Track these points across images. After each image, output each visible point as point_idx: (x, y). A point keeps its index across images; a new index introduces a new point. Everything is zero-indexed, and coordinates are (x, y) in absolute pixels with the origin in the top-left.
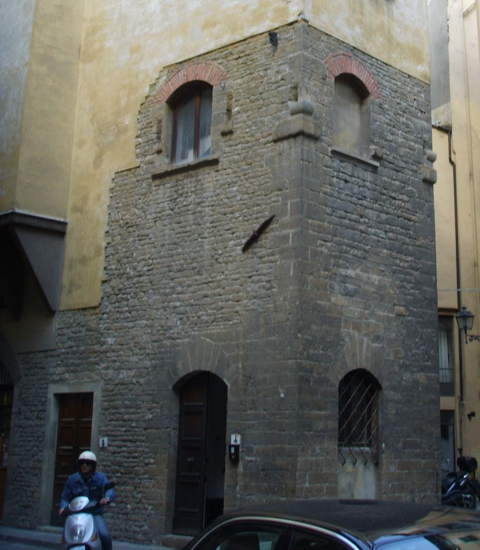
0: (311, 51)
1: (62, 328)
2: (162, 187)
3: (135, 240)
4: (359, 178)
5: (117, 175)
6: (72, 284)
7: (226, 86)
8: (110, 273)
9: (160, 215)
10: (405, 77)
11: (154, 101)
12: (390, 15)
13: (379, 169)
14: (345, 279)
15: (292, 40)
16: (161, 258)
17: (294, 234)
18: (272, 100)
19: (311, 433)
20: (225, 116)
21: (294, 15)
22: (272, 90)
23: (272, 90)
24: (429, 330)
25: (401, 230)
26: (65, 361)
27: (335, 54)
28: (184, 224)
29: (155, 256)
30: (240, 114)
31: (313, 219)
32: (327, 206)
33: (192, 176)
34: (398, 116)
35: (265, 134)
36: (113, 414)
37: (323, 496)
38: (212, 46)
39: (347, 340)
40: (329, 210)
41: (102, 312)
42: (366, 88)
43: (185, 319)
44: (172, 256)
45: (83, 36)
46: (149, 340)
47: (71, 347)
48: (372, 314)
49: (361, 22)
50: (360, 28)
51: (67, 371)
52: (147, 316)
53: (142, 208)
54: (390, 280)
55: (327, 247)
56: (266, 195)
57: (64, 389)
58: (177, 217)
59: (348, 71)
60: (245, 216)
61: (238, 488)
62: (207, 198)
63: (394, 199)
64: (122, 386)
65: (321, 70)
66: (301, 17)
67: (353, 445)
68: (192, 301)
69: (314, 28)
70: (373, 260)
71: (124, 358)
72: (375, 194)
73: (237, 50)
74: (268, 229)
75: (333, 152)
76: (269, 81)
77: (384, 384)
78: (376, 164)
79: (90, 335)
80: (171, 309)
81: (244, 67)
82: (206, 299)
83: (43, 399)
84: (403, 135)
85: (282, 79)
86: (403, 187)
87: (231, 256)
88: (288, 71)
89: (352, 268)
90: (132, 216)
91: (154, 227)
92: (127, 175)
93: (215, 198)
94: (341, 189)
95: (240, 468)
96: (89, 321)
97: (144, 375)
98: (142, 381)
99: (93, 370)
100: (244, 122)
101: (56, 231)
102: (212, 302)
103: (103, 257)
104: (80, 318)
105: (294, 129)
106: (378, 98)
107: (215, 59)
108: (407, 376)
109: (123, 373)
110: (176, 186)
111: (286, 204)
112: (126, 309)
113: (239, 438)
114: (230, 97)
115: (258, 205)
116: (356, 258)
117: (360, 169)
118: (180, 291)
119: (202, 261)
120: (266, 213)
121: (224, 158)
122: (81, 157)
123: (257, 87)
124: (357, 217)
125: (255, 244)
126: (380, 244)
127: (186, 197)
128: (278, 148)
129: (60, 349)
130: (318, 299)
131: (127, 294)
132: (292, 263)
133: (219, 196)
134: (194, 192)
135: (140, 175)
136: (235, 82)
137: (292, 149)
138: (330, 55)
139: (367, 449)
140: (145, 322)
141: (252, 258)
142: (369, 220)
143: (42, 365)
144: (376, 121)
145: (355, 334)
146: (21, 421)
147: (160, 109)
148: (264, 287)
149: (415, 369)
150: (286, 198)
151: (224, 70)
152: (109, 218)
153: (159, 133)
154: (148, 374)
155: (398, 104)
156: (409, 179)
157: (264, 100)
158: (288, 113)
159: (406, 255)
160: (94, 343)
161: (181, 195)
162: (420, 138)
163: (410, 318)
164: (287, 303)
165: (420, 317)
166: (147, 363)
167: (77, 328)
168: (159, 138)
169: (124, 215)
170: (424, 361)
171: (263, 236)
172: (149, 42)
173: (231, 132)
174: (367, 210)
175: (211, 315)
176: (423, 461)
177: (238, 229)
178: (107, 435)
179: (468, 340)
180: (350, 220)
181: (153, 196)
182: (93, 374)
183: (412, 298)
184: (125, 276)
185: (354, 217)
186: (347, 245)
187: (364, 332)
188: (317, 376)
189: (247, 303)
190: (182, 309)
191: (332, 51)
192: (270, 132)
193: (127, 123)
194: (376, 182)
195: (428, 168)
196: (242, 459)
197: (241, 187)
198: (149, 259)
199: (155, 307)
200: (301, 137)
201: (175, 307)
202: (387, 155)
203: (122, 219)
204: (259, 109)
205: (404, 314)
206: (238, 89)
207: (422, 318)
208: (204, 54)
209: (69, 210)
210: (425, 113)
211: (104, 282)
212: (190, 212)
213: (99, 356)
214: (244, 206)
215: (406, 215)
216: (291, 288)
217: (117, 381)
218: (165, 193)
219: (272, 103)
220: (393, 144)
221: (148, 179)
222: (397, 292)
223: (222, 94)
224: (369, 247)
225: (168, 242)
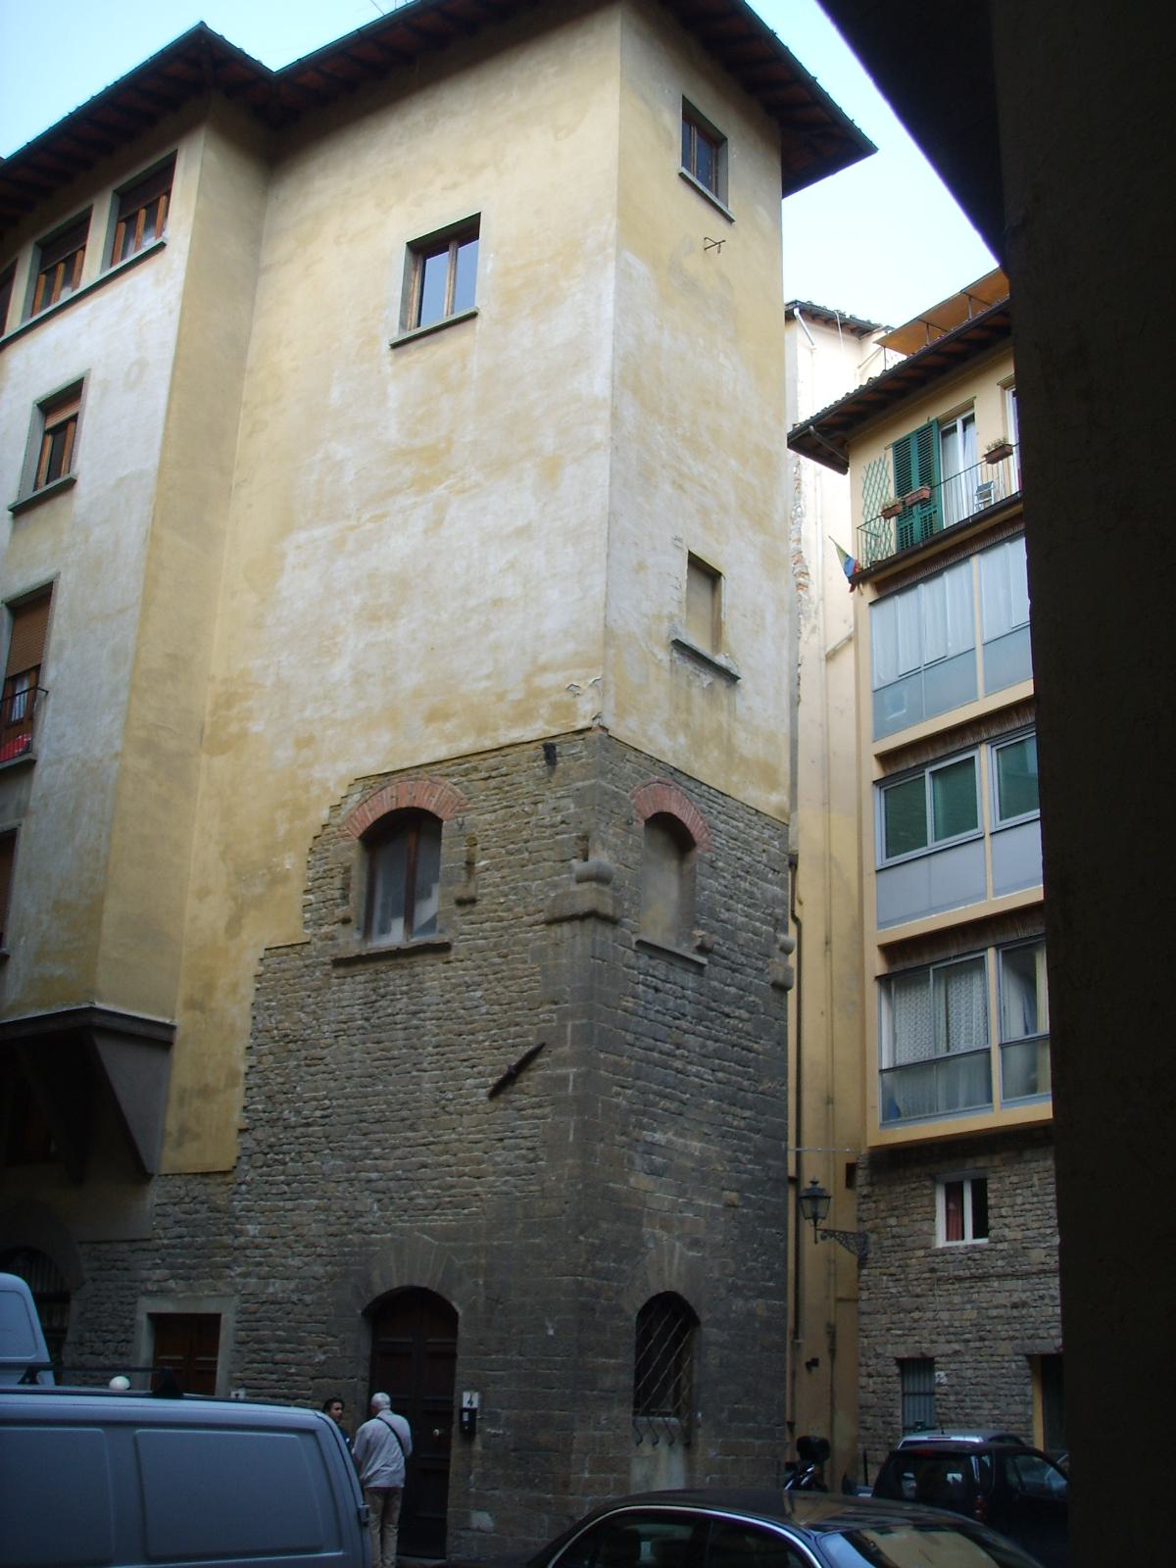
0: (612, 779)
1: (165, 1204)
2: (349, 979)
3: (299, 1066)
4: (675, 984)
5: (268, 952)
6: (184, 1131)
7: (466, 822)
9: (345, 1026)
10: (751, 815)
11: (338, 833)
12: (732, 711)
13: (707, 968)
14: (651, 1147)
15: (580, 758)
16: (346, 1099)
17: (577, 1076)
18: (545, 854)
19: (595, 1393)
20: (463, 872)
21: (585, 717)
22: (544, 838)
23: (544, 838)
24: (774, 1231)
25: (738, 1067)
26: (168, 1260)
27: (648, 781)
28: (387, 1044)
29: (336, 1093)
30: (489, 873)
31: (607, 1052)
32: (627, 1031)
33: (403, 967)
34: (738, 879)
35: (531, 909)
36: (254, 1351)
37: (609, 1493)
38: (442, 752)
39: (651, 1245)
40: (630, 1037)
41: (239, 1181)
42: (691, 835)
43: (386, 1201)
45: (209, 706)
46: (323, 1232)
48: (690, 1204)
49: (686, 726)
50: (686, 736)
52: (319, 1193)
53: (314, 1012)
54: (718, 1149)
55: (626, 1097)
56: (530, 1009)
57: (167, 1307)
58: (374, 1032)
59: (665, 810)
60: (494, 1041)
61: (472, 1477)
62: (429, 1006)
63: (728, 1016)
64: (272, 1306)
65: (625, 810)
66: (597, 721)
67: (653, 1414)
68: (400, 1172)
69: (617, 739)
70: (693, 1117)
72: (699, 1009)
73: (485, 764)
74: (533, 1065)
75: (640, 943)
76: (540, 823)
77: (704, 1316)
78: (703, 960)
79: (216, 1219)
80: (363, 1183)
81: (497, 794)
82: (423, 1170)
83: (127, 1322)
84: (744, 911)
85: (563, 822)
86: (742, 997)
87: (468, 1103)
88: (572, 811)
89: (662, 1131)
90: (295, 1023)
91: (334, 1047)
92: (287, 955)
94: (648, 1002)
96: (214, 1195)
97: (312, 1289)
98: (308, 1298)
99: (220, 1277)
101: (157, 1039)
102: (434, 1176)
103: (240, 1090)
104: (197, 1188)
105: (583, 905)
106: (709, 850)
107: (447, 775)
108: (738, 1304)
109: (274, 1284)
110: (375, 980)
111: (565, 1026)
112: (282, 1178)
113: (476, 1397)
115: (517, 1025)
116: (667, 1113)
117: (678, 970)
118: (377, 1156)
119: (417, 1108)
120: (531, 1039)
121: (461, 942)
122: (204, 916)
123: (518, 831)
124: (672, 1047)
125: (510, 1088)
126: (703, 1090)
127: (392, 1000)
128: (553, 935)
129: (160, 1239)
130: (610, 1181)
131: (284, 1153)
132: (572, 1122)
133: (449, 1005)
134: (406, 993)
135: (311, 957)
136: (482, 817)
137: (577, 939)
138: (638, 783)
139: (674, 1420)
140: (315, 1202)
141: (506, 1109)
142: (689, 1051)
143: (126, 1264)
144: (704, 889)
145: (663, 1236)
146: (85, 1357)
147: (349, 849)
148: (524, 1157)
149: (751, 1294)
150: (565, 1015)
151: (463, 795)
152: (254, 1024)
153: (346, 887)
154: (320, 1288)
155: (739, 859)
156: (751, 982)
157: (530, 853)
158: (572, 878)
159: (742, 1108)
160: (223, 1231)
162: (770, 915)
163: (745, 1211)
164: (562, 1186)
165: (760, 1208)
167: (192, 1205)
168: (345, 897)
169: (281, 1022)
170: (763, 1280)
171: (524, 1075)
172: (330, 732)
173: (473, 901)
174: (687, 1035)
175: (432, 1197)
177: (482, 1061)
178: (246, 1387)
179: (818, 1236)
181: (334, 993)
182: (220, 1284)
183: (750, 1177)
184: (280, 1123)
185: (667, 1047)
186: (656, 1093)
187: (676, 1233)
188: (606, 1302)
189: (495, 1181)
190: (381, 1185)
191: (642, 777)
192: (540, 907)
193: (288, 867)
194: (701, 990)
195: (780, 965)
196: (480, 1431)
197: (489, 992)
198: (325, 1098)
199: (333, 1178)
200: (593, 920)
201: (369, 1181)
202: (719, 944)
203: (277, 1028)
204: (523, 866)
205: (736, 1203)
206: (487, 830)
207: (764, 1210)
209: (179, 1006)
210: (779, 872)
211: (242, 1131)
212: (399, 1026)
213: (231, 1254)
214: (492, 1024)
215: (745, 1043)
216: (570, 1161)
217: (264, 1298)
218: (354, 991)
219: (544, 860)
220: (729, 927)
221: (325, 964)
222: (728, 1169)
223: (459, 836)
224: (688, 1096)
225: (359, 1072)
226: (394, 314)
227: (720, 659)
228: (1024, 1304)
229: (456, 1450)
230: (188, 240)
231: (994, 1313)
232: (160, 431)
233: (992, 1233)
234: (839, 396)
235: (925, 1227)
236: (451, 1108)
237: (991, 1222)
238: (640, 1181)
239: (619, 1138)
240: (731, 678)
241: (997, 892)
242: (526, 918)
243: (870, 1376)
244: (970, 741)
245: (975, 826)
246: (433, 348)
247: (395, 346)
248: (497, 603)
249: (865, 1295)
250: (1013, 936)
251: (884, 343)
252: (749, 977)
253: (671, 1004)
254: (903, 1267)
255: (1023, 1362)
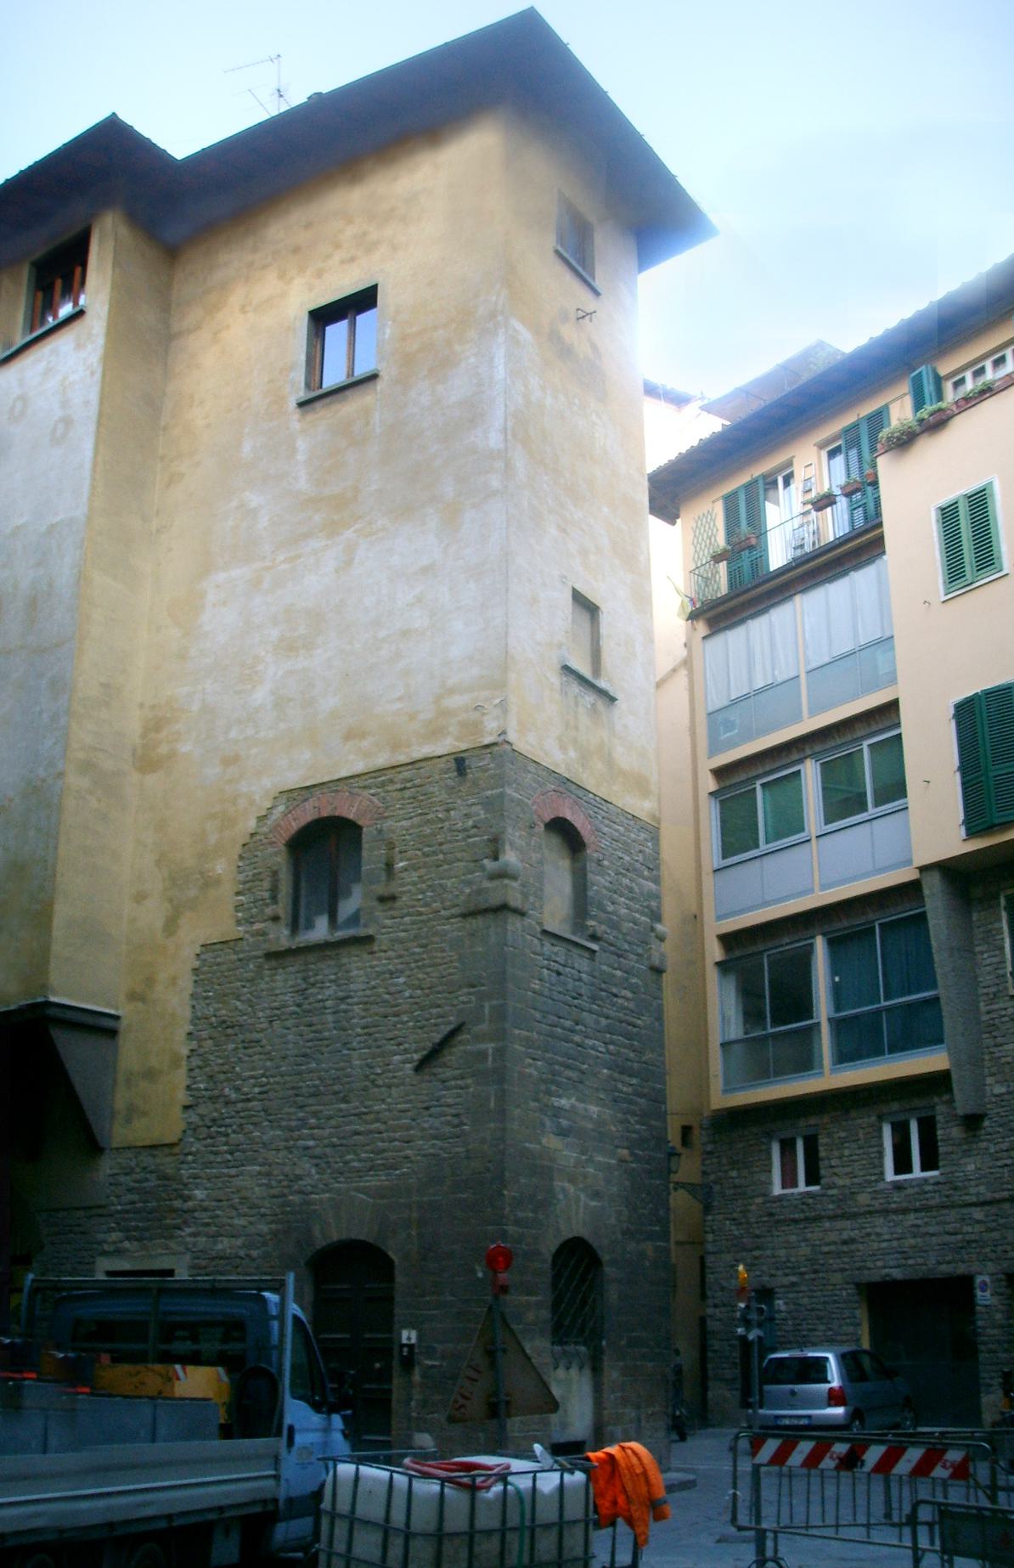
8: (197, 1093)
14: (558, 1112)
18: (459, 855)
29: (273, 1071)
33: (330, 958)
38: (360, 766)
39: (561, 1197)
40: (538, 1015)
44: (300, 1073)
47: (133, 1203)
48: (590, 1160)
51: (128, 1238)
55: (537, 1069)
61: (413, 1403)
71: (225, 1220)
77: (605, 1257)
85: (475, 827)
93: (368, 992)
95: (417, 1377)
98: (255, 1253)
99: (171, 1237)
100: (414, 884)
101: (103, 1028)
103: (183, 1071)
104: (146, 1159)
113: (414, 1334)
114: (391, 846)
123: (434, 834)
135: (243, 951)
147: (276, 854)
148: (448, 1123)
153: (274, 891)
154: (265, 1244)
161: (313, 985)
166: (263, 1228)
168: (274, 899)
171: (446, 1052)
172: (254, 751)
173: (393, 898)
176: (650, 1365)
180: (564, 1028)
182: (172, 1244)
185: (568, 1023)
190: (318, 1151)
198: (263, 1076)
201: (307, 1148)
208: (347, 778)
211: (186, 1108)
218: (286, 981)
226: (299, 375)
227: (602, 683)
228: (853, 1241)
229: (397, 1381)
230: (106, 308)
231: (826, 1249)
232: (87, 482)
233: (823, 1181)
234: (673, 456)
235: (763, 1178)
236: (380, 1082)
237: (823, 1172)
238: (552, 1142)
239: (533, 1104)
240: (613, 699)
241: (823, 887)
242: (443, 912)
243: (716, 1306)
244: (795, 756)
245: (802, 829)
246: (335, 407)
247: (301, 405)
248: (406, 634)
249: (710, 1237)
250: (838, 925)
251: (707, 409)
252: (631, 961)
253: (570, 987)
254: (745, 1212)
255: (852, 1290)
